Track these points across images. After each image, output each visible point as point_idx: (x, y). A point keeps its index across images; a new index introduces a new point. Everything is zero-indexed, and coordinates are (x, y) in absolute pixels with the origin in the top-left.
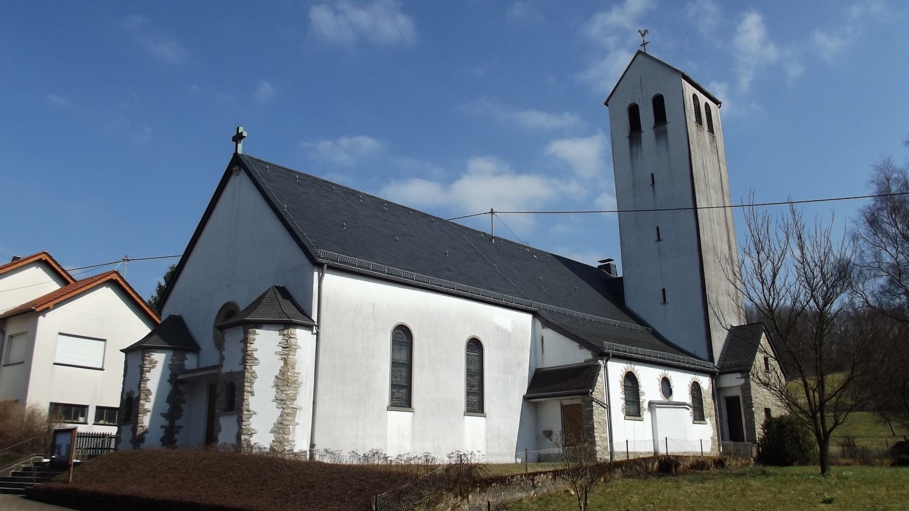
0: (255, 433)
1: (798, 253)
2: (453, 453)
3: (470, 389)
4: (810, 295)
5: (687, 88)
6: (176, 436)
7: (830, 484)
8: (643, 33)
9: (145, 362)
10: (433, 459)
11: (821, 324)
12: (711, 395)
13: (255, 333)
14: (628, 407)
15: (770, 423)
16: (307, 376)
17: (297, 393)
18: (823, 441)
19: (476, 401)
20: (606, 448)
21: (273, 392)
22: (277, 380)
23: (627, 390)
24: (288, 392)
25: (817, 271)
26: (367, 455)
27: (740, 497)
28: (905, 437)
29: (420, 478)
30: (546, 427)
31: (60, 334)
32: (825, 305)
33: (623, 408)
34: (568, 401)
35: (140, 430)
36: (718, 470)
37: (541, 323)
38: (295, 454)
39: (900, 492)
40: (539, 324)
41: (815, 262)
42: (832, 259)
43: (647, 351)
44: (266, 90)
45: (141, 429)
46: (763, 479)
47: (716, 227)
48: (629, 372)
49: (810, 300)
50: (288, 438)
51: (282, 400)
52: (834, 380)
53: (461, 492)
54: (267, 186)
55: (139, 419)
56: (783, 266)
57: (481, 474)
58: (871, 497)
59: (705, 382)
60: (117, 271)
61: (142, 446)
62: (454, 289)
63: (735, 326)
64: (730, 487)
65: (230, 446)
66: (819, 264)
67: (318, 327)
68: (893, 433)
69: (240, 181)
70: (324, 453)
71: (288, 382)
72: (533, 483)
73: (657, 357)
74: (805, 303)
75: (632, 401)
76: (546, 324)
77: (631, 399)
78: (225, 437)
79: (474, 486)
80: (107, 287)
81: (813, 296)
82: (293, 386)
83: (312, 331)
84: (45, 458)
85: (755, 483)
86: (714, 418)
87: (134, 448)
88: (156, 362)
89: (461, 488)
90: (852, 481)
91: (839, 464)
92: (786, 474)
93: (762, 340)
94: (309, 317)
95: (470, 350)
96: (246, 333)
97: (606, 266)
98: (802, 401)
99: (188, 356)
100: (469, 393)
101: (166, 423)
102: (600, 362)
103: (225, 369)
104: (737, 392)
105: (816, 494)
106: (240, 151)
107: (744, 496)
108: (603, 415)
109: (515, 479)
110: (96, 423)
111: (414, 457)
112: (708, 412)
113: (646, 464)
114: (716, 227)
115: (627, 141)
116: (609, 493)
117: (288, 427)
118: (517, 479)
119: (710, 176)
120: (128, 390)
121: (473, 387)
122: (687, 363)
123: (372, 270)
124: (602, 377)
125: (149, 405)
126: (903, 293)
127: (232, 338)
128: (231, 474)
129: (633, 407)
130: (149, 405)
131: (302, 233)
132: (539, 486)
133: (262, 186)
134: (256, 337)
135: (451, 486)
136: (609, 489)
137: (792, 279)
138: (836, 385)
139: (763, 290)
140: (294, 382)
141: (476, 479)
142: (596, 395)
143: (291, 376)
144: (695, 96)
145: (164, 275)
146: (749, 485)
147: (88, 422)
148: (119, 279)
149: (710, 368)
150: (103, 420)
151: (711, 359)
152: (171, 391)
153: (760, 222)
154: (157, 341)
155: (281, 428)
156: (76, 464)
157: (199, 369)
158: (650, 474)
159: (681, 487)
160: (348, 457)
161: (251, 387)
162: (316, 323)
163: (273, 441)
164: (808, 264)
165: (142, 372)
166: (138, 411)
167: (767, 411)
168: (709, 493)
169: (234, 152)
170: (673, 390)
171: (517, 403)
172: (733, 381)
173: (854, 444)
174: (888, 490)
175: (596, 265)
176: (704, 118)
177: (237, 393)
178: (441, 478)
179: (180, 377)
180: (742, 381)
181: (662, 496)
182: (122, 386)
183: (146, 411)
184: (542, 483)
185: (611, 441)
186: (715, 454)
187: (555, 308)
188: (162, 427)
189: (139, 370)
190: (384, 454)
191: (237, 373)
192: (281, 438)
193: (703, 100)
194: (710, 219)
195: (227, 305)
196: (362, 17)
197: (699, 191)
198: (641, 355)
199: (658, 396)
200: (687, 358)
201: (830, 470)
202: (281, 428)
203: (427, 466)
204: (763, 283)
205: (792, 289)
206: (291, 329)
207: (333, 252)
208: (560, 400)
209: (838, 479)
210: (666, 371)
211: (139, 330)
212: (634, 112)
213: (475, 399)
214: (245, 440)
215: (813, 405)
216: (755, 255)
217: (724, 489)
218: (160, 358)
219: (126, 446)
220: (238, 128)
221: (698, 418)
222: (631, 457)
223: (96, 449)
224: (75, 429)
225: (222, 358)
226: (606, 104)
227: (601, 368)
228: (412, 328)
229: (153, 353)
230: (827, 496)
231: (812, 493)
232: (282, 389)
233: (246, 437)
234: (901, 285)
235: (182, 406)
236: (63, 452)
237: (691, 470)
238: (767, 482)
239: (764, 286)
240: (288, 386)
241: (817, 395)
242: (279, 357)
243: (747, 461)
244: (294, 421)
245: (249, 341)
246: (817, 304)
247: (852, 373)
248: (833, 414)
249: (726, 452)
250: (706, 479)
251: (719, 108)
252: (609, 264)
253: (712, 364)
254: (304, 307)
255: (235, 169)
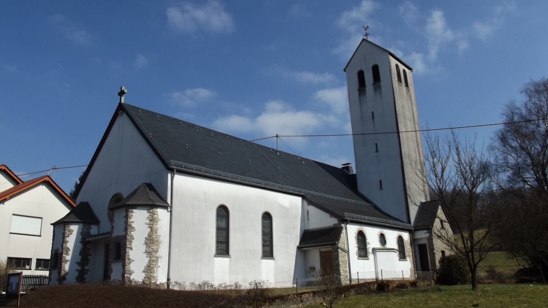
0: (133, 273)
1: (456, 158)
2: (252, 282)
3: (265, 243)
4: (464, 183)
5: (392, 61)
6: (86, 276)
7: (477, 295)
8: (365, 28)
9: (66, 231)
10: (240, 286)
11: (471, 200)
12: (409, 243)
13: (132, 212)
14: (360, 252)
15: (444, 259)
16: (165, 237)
17: (159, 248)
18: (473, 270)
19: (268, 250)
20: (347, 277)
21: (144, 248)
22: (146, 240)
23: (359, 242)
24: (153, 247)
25: (468, 169)
26: (200, 284)
27: (424, 304)
28: (524, 266)
29: (232, 298)
30: (311, 265)
31: (13, 215)
32: (473, 188)
33: (357, 253)
34: (324, 249)
35: (63, 273)
36: (413, 289)
37: (307, 202)
38: (157, 285)
39: (518, 299)
40: (306, 203)
41: (466, 163)
42: (476, 161)
43: (371, 218)
44: (141, 61)
45: (63, 272)
46: (438, 293)
47: (411, 143)
48: (360, 231)
49: (464, 186)
50: (154, 275)
51: (149, 252)
52: (479, 233)
53: (257, 305)
54: (139, 122)
55: (62, 266)
56: (448, 166)
57: (269, 294)
58: (501, 302)
59: (406, 236)
60: (48, 175)
61: (64, 282)
62: (254, 183)
63: (423, 202)
64: (419, 298)
65: (117, 281)
66: (469, 165)
67: (171, 207)
68: (519, 264)
69: (123, 120)
70: (174, 284)
71: (153, 241)
72: (301, 299)
73: (377, 222)
74: (461, 188)
75: (363, 248)
76: (310, 203)
77: (362, 247)
78: (115, 276)
79: (265, 302)
80: (42, 186)
81: (465, 184)
82: (156, 243)
83: (168, 210)
84: (3, 292)
85: (434, 296)
86: (411, 257)
87: (59, 284)
88: (73, 231)
89: (257, 303)
90: (490, 293)
91: (484, 283)
92: (452, 290)
93: (439, 210)
94: (166, 202)
95: (264, 219)
96: (127, 212)
97: (347, 167)
98: (460, 245)
99: (92, 226)
100: (264, 246)
101: (79, 268)
102: (343, 225)
103: (114, 235)
104: (425, 242)
105: (469, 302)
106: (123, 101)
107: (427, 303)
108: (345, 257)
109: (290, 297)
110: (37, 269)
111: (229, 285)
112: (408, 253)
113: (369, 285)
114: (411, 143)
115: (357, 92)
116: (347, 304)
117: (154, 268)
118: (291, 297)
119: (407, 113)
120: (55, 248)
121: (266, 241)
122: (395, 225)
123: (204, 172)
124: (344, 234)
125: (68, 257)
126: (522, 181)
127: (119, 215)
128: (117, 298)
129: (363, 252)
130: (68, 257)
131: (161, 150)
132: (304, 301)
133: (137, 122)
134: (133, 214)
135: (251, 302)
136: (347, 302)
137: (453, 174)
138: (480, 236)
139: (436, 181)
140: (157, 241)
141: (266, 297)
142: (340, 245)
143: (155, 237)
144: (397, 66)
145: (79, 177)
146: (430, 297)
147: (32, 268)
148: (50, 180)
149: (409, 227)
150: (41, 267)
151: (409, 222)
152: (82, 249)
153: (433, 140)
154: (73, 218)
155: (149, 269)
156: (22, 295)
157: (99, 235)
158: (372, 292)
159: (390, 299)
160: (189, 286)
161: (130, 244)
162: (170, 205)
163: (144, 277)
164: (463, 165)
165: (64, 237)
166: (62, 261)
167: (443, 252)
168: (406, 302)
169: (119, 102)
170: (387, 241)
171: (293, 251)
172: (422, 235)
173: (494, 271)
174: (511, 298)
175: (340, 166)
176: (403, 78)
177: (122, 249)
178: (245, 298)
179: (87, 240)
180: (428, 235)
181: (378, 305)
182: (52, 246)
183: (67, 261)
184: (307, 299)
185: (350, 272)
186: (413, 279)
187: (316, 193)
188: (77, 270)
189: (62, 236)
190: (211, 284)
191: (122, 236)
192: (149, 275)
193: (402, 67)
194: (407, 138)
195: (115, 195)
196: (200, 14)
197: (400, 122)
198: (368, 220)
199: (378, 245)
200: (395, 222)
201: (477, 287)
202: (149, 269)
203: (237, 290)
204: (436, 176)
205: (453, 179)
206: (155, 209)
207: (180, 161)
208: (319, 248)
209: (482, 292)
210: (383, 230)
211: (63, 211)
212: (361, 75)
213: (268, 249)
214: (127, 277)
215: (467, 249)
216: (431, 159)
217: (415, 300)
218: (75, 228)
219: (55, 283)
220: (121, 88)
221: (402, 258)
222: (362, 282)
223: (35, 285)
224: (21, 273)
225: (113, 228)
226: (345, 70)
227: (343, 229)
228: (228, 207)
229: (70, 225)
230: (475, 302)
231: (466, 301)
232: (149, 245)
233: (128, 275)
234: (520, 176)
235: (89, 257)
236: (14, 288)
237: (396, 289)
238: (441, 295)
239: (437, 178)
240: (153, 243)
241: (469, 242)
242: (147, 226)
243: (430, 283)
244: (157, 265)
245: (129, 217)
246: (468, 188)
247: (489, 229)
248: (479, 254)
249: (418, 278)
250: (405, 294)
251: (412, 72)
252: (348, 166)
253: (409, 225)
254: (162, 195)
255: (120, 112)
